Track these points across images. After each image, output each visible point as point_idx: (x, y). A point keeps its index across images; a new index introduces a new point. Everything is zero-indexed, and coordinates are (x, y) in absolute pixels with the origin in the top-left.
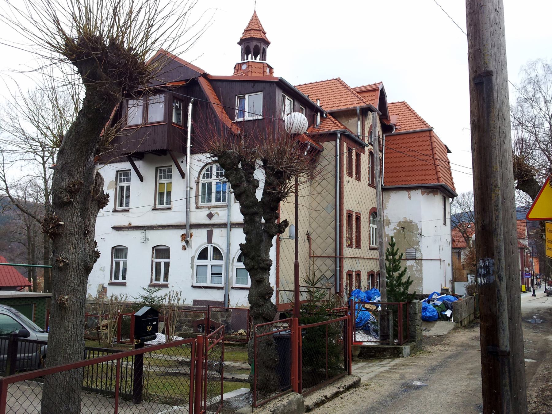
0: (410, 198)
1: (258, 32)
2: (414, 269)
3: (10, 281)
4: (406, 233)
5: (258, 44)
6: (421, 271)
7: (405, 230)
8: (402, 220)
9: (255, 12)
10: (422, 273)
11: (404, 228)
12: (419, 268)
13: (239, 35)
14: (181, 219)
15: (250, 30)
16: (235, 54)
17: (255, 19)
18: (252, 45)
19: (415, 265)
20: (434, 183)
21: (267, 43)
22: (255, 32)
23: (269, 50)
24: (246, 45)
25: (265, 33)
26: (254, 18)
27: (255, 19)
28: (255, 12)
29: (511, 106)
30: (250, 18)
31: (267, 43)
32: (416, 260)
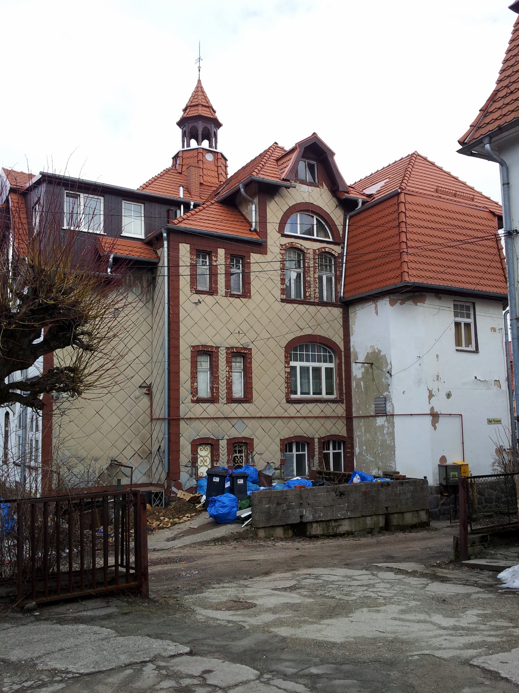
0: (377, 313)
1: (207, 109)
2: (385, 432)
3: (433, 187)
4: (375, 372)
5: (209, 126)
6: (392, 434)
7: (373, 367)
8: (370, 352)
9: (199, 81)
10: (393, 438)
11: (372, 364)
12: (391, 430)
13: (179, 115)
14: (124, 420)
15: (197, 105)
16: (173, 141)
17: (199, 91)
18: (200, 126)
19: (386, 424)
20: (396, 283)
21: (218, 125)
22: (204, 108)
23: (220, 132)
24: (191, 125)
25: (215, 112)
26: (200, 89)
27: (199, 91)
28: (199, 81)
29: (343, 640)
30: (193, 89)
31: (218, 125)
32: (387, 415)
